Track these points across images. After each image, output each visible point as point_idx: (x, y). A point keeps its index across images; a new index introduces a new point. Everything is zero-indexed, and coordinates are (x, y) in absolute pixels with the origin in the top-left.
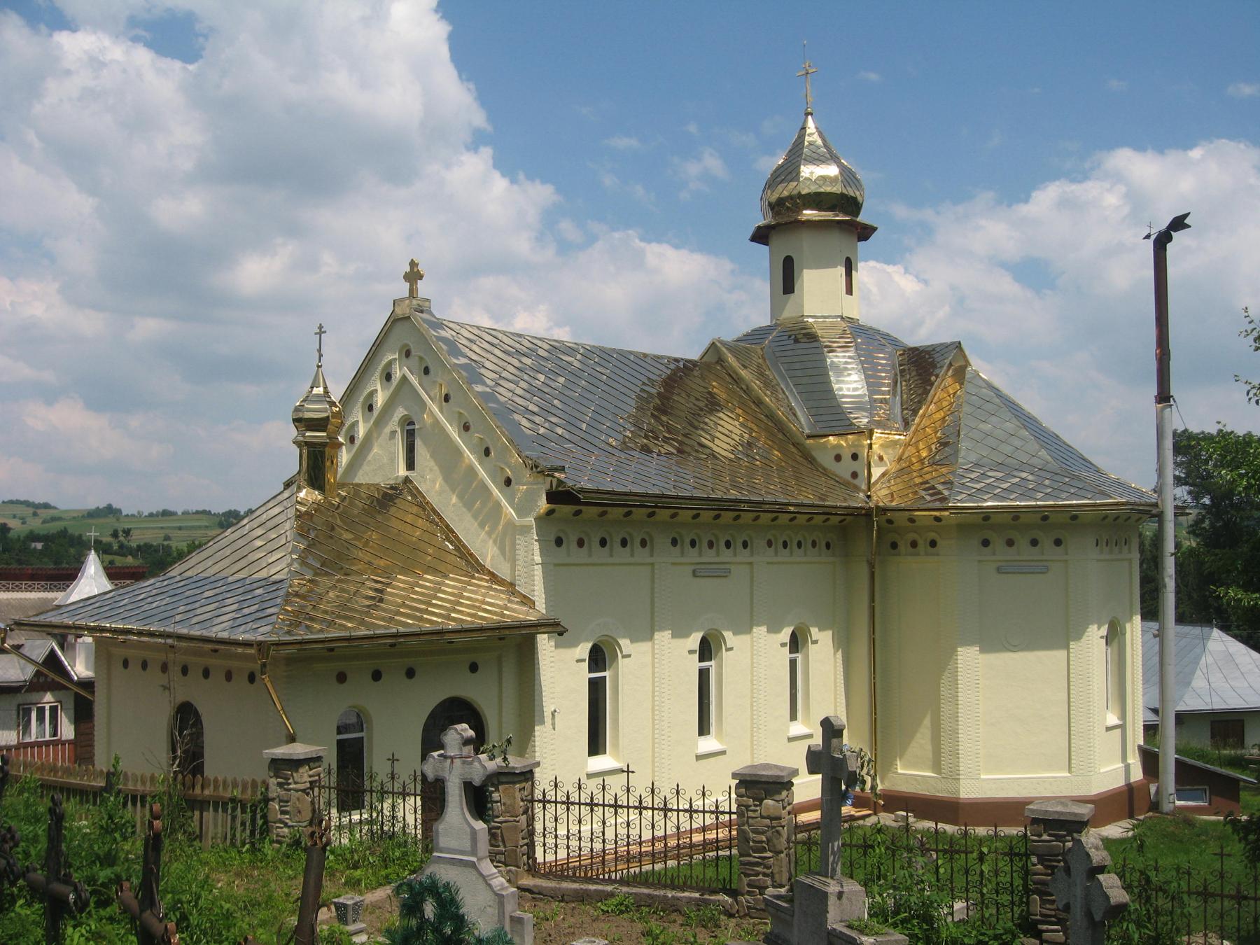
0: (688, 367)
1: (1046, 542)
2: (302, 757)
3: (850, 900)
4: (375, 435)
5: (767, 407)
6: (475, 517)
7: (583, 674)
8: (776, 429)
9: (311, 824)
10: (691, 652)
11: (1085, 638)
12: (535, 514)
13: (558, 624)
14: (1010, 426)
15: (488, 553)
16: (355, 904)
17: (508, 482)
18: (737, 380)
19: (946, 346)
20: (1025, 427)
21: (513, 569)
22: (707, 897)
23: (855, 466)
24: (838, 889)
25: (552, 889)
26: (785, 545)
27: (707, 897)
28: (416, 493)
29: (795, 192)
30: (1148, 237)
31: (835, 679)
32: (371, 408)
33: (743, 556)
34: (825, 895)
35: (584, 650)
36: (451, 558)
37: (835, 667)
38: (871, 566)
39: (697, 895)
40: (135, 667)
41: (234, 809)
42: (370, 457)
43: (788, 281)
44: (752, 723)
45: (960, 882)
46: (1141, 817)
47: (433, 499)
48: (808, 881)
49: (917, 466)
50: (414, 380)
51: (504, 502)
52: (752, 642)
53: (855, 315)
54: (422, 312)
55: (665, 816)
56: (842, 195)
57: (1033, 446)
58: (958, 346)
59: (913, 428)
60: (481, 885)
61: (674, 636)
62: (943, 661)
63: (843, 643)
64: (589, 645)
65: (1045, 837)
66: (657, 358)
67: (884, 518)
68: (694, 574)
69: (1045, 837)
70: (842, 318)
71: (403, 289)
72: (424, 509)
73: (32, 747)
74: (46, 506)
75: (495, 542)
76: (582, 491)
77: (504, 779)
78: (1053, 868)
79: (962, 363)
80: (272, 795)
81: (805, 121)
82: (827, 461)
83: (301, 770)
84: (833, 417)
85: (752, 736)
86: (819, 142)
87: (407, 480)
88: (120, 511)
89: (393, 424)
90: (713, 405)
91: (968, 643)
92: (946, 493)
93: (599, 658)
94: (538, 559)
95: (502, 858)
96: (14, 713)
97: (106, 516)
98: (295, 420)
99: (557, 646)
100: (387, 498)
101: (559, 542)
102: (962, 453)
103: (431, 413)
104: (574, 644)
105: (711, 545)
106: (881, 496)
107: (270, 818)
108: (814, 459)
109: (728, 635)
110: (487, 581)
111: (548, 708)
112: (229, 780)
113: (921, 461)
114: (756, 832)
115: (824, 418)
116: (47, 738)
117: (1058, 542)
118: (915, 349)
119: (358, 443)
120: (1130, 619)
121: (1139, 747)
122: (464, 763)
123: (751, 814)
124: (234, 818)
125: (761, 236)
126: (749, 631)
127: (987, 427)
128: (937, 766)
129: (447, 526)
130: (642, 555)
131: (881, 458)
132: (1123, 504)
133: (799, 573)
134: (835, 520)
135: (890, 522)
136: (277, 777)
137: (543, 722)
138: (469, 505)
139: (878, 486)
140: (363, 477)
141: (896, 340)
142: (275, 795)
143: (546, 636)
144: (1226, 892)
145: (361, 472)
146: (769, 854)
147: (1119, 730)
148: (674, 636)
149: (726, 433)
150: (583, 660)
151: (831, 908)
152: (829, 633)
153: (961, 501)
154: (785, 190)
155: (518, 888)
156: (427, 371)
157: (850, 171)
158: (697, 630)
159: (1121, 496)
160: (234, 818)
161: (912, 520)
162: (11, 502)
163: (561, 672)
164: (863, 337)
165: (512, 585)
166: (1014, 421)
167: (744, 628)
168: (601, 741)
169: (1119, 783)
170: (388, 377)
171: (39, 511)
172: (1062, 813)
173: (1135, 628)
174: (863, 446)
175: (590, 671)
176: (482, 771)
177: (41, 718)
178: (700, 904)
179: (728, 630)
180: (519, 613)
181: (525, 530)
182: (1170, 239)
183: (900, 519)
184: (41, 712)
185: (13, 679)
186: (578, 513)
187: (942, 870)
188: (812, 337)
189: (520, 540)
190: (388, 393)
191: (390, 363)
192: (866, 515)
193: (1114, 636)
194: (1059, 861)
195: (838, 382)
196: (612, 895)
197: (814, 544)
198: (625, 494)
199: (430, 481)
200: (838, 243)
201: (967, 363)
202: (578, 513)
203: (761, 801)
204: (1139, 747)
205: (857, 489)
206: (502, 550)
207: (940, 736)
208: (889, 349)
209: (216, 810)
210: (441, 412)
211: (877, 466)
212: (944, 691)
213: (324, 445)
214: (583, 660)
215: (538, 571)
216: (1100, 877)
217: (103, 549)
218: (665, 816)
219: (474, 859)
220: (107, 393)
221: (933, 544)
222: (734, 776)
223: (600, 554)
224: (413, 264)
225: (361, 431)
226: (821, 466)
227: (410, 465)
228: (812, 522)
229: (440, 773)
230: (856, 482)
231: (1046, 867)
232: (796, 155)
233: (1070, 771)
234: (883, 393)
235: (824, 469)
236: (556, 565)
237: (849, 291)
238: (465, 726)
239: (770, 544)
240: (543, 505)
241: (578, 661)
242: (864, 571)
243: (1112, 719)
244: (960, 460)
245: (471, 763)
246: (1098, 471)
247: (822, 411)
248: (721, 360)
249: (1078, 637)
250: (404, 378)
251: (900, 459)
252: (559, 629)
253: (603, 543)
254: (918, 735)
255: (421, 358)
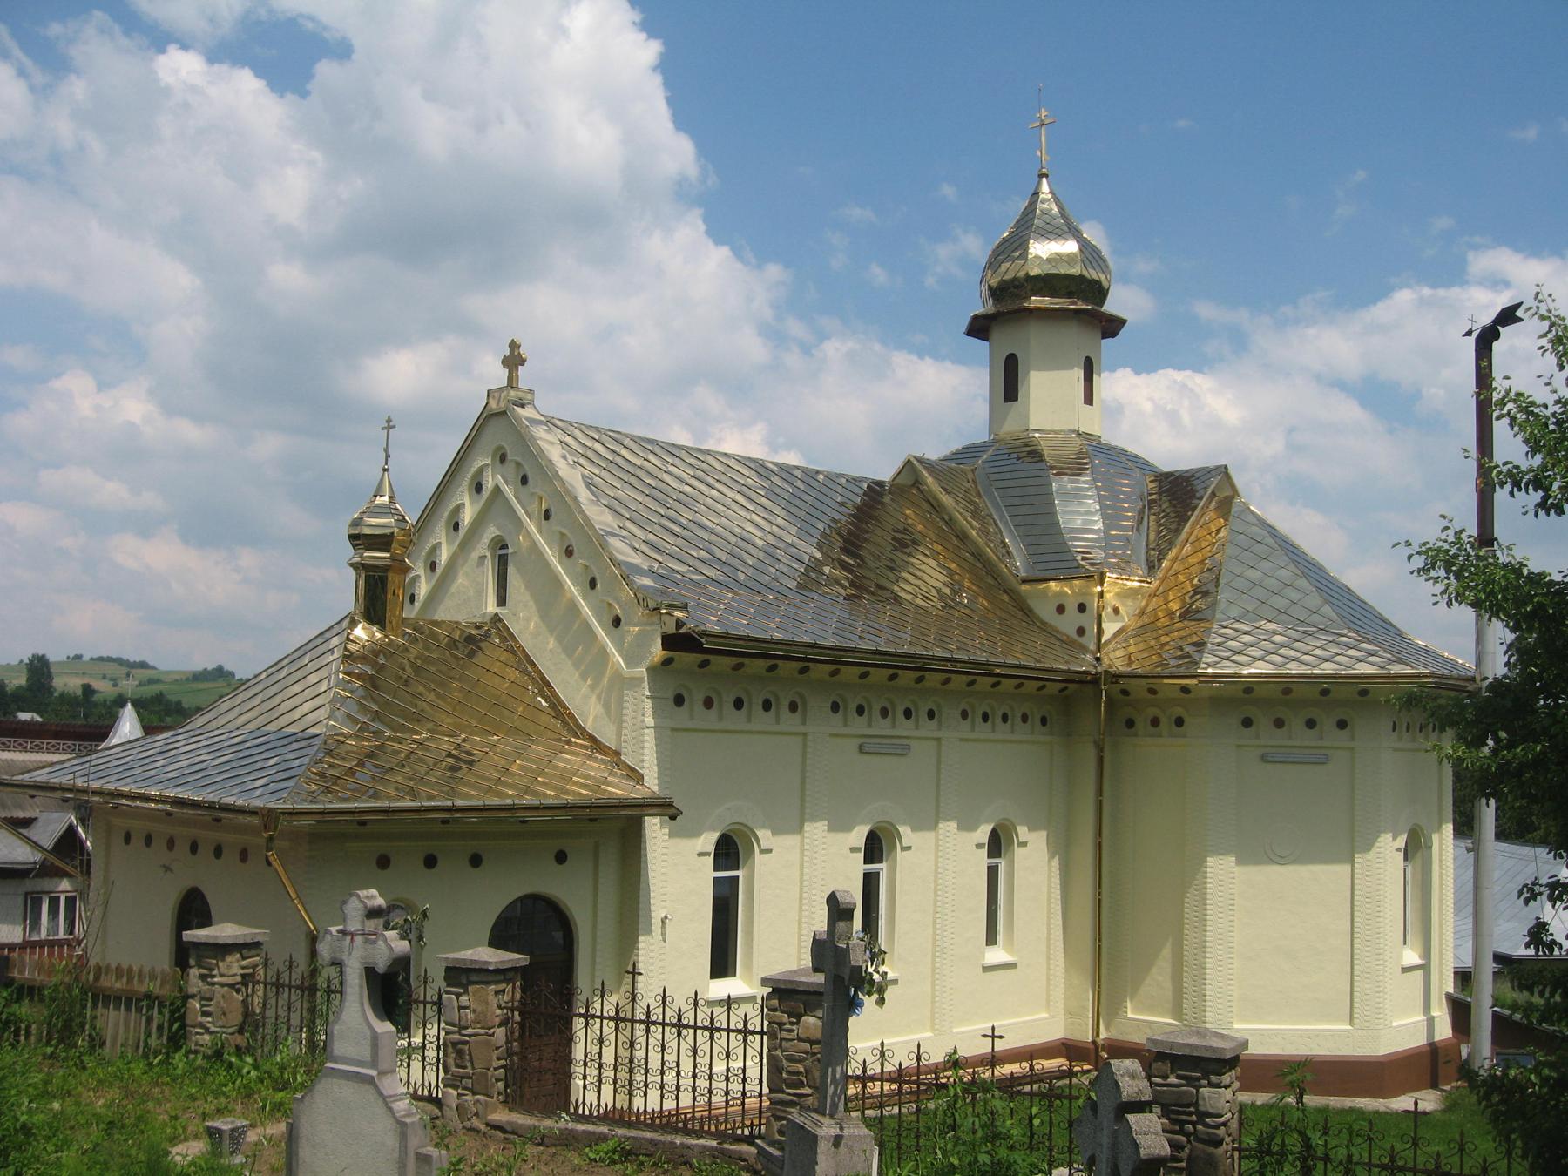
0: (875, 491)
1: (1328, 723)
2: (230, 941)
3: (850, 1148)
4: (460, 561)
5: (974, 543)
6: (576, 665)
7: (707, 872)
8: (983, 570)
9: (241, 1031)
10: (853, 850)
11: (1375, 850)
12: (647, 663)
13: (671, 805)
14: (1283, 573)
15: (590, 712)
16: (234, 1130)
17: (617, 622)
18: (936, 507)
19: (1208, 472)
20: (1305, 576)
21: (619, 735)
22: (726, 1146)
23: (1082, 620)
24: (835, 1131)
25: (529, 1128)
26: (985, 717)
27: (726, 1146)
28: (507, 636)
29: (1021, 274)
30: (1469, 333)
31: (1049, 892)
32: (456, 527)
33: (929, 728)
34: (814, 1139)
35: (708, 841)
36: (544, 718)
37: (1050, 877)
38: (1100, 749)
39: (714, 1143)
40: (138, 842)
41: (150, 1007)
42: (453, 589)
43: (1010, 386)
44: (934, 945)
45: (1060, 1140)
46: (1447, 1088)
47: (526, 641)
48: (800, 1120)
49: (1165, 621)
50: (508, 491)
51: (611, 648)
52: (937, 840)
53: (1096, 431)
54: (523, 406)
55: (679, 1034)
56: (1082, 277)
57: (1314, 600)
58: (1223, 471)
59: (1160, 574)
60: (379, 1109)
61: (831, 829)
62: (1188, 875)
63: (1062, 847)
64: (716, 835)
65: (1172, 1080)
66: (856, 480)
67: (1116, 688)
68: (861, 749)
69: (1172, 1080)
70: (1078, 433)
71: (500, 376)
72: (515, 654)
73: (42, 947)
74: (143, 665)
75: (599, 698)
76: (706, 634)
77: (474, 978)
78: (1182, 1123)
79: (1228, 493)
80: (192, 990)
81: (1039, 184)
82: (1046, 612)
83: (229, 959)
84: (1055, 557)
85: (934, 962)
86: (1055, 210)
87: (496, 619)
88: (232, 674)
89: (482, 547)
90: (905, 542)
91: (1222, 851)
92: (1196, 656)
93: (729, 851)
94: (650, 720)
95: (469, 1083)
96: (20, 900)
97: (214, 680)
98: (352, 537)
99: (671, 835)
100: (471, 642)
101: (679, 700)
102: (1222, 605)
103: (528, 534)
104: (694, 833)
105: (884, 713)
106: (1115, 659)
107: (188, 1022)
108: (1031, 611)
109: (904, 830)
110: (586, 748)
111: (657, 913)
112: (146, 970)
113: (1171, 614)
114: (790, 1059)
115: (1043, 558)
116: (61, 935)
117: (1342, 724)
118: (1170, 474)
119: (439, 570)
120: (1439, 829)
121: (1448, 996)
122: (366, 941)
123: (785, 1035)
124: (149, 1020)
125: (979, 328)
126: (934, 827)
127: (1254, 575)
128: (1177, 1011)
129: (543, 678)
130: (790, 721)
131: (1116, 611)
132: (1425, 676)
133: (1005, 756)
134: (1053, 688)
135: (1125, 692)
136: (200, 967)
137: (649, 932)
138: (569, 651)
139: (1111, 647)
140: (443, 613)
141: (1147, 463)
142: (195, 990)
143: (657, 820)
144: (1375, 1161)
145: (442, 608)
146: (807, 1091)
147: (1420, 973)
148: (831, 829)
149: (926, 576)
150: (708, 854)
151: (821, 1158)
152: (1044, 833)
153: (1210, 665)
154: (1009, 270)
155: (488, 1125)
156: (524, 480)
157: (1094, 248)
158: (863, 822)
159: (1426, 666)
160: (149, 1020)
161: (1152, 691)
162: (101, 659)
163: (677, 869)
164: (1094, 456)
165: (618, 754)
166: (1292, 567)
167: (927, 822)
168: (730, 960)
169: (1419, 1040)
170: (479, 488)
171: (134, 671)
172: (1196, 1047)
173: (1444, 841)
174: (1092, 595)
175: (716, 869)
176: (387, 952)
177: (54, 911)
178: (715, 1154)
179: (904, 824)
180: (619, 789)
181: (634, 682)
182: (1497, 336)
183: (1138, 688)
184: (54, 903)
185: (20, 859)
186: (704, 664)
187: (1036, 1122)
188: (1036, 456)
189: (629, 696)
190: (478, 507)
191: (481, 471)
192: (1091, 681)
193: (1415, 848)
194: (1190, 1114)
195: (1065, 512)
196: (603, 1138)
197: (1025, 718)
198: (764, 641)
199: (525, 622)
200: (1076, 339)
201: (1235, 493)
202: (704, 664)
203: (799, 1017)
204: (1448, 996)
205: (1084, 649)
206: (607, 707)
207: (1182, 971)
208: (1137, 474)
209: (128, 1009)
210: (540, 532)
211: (1110, 621)
212: (1189, 913)
213: (387, 568)
214: (708, 854)
215: (649, 737)
216: (1131, 1118)
217: (139, 705)
218: (679, 1034)
219: (373, 1073)
220: (213, 525)
221: (1180, 722)
222: (765, 982)
223: (736, 719)
224: (514, 346)
225: (444, 556)
226: (1038, 618)
227: (501, 600)
228: (1023, 690)
229: (338, 955)
230: (1082, 640)
231: (1173, 1121)
232: (1026, 227)
233: (1351, 1022)
234: (1124, 528)
235: (1044, 623)
236: (673, 730)
237: (1089, 399)
238: (374, 892)
239: (964, 715)
240: (657, 652)
241: (700, 854)
242: (1091, 752)
243: (1412, 957)
244: (1218, 616)
245: (375, 942)
246: (1400, 634)
247: (1042, 549)
248: (917, 482)
249: (1367, 847)
250: (497, 489)
251: (1142, 613)
252: (673, 811)
253: (739, 704)
254: (1154, 970)
255: (518, 464)
